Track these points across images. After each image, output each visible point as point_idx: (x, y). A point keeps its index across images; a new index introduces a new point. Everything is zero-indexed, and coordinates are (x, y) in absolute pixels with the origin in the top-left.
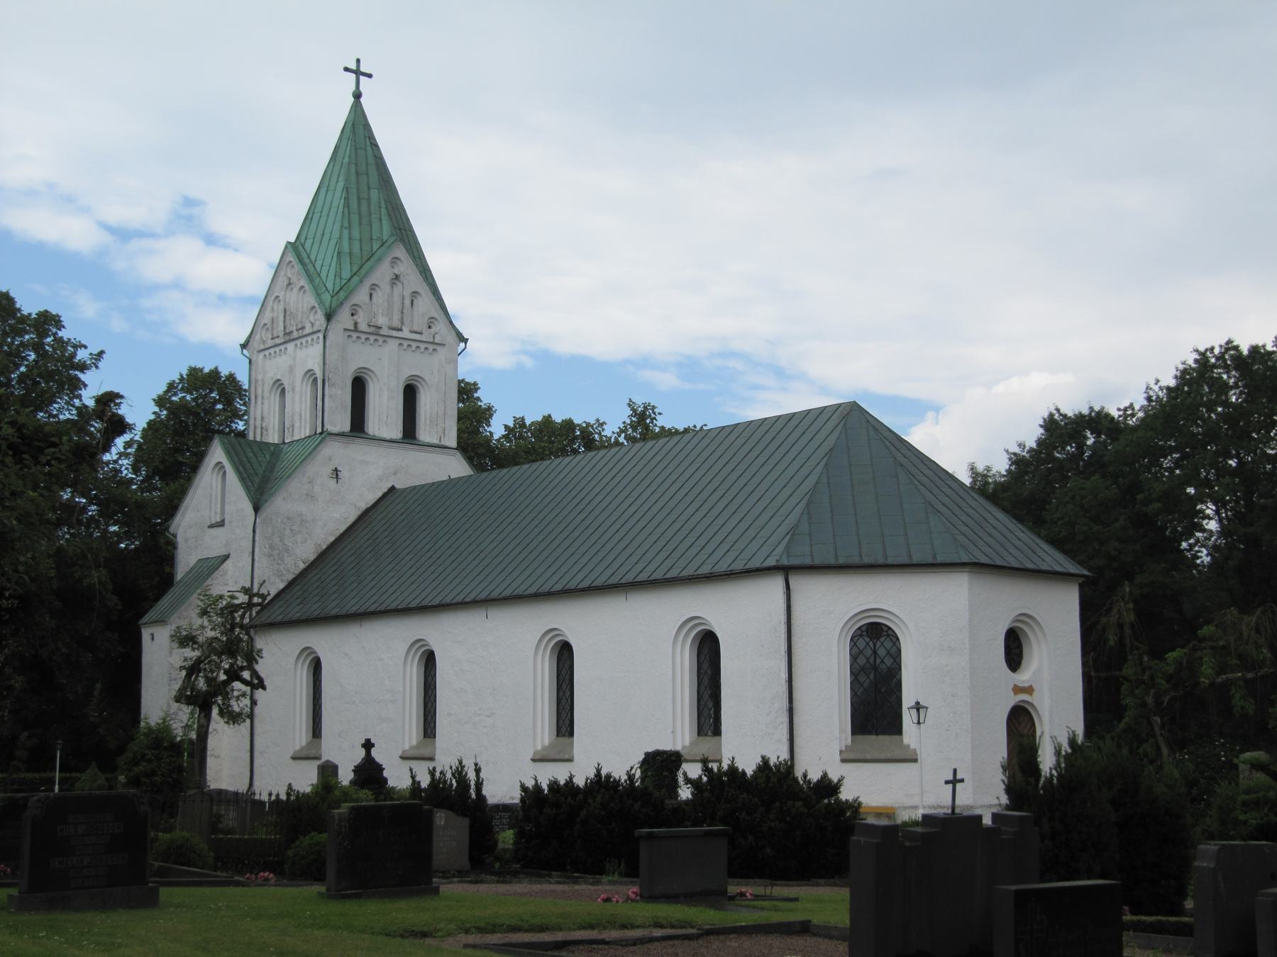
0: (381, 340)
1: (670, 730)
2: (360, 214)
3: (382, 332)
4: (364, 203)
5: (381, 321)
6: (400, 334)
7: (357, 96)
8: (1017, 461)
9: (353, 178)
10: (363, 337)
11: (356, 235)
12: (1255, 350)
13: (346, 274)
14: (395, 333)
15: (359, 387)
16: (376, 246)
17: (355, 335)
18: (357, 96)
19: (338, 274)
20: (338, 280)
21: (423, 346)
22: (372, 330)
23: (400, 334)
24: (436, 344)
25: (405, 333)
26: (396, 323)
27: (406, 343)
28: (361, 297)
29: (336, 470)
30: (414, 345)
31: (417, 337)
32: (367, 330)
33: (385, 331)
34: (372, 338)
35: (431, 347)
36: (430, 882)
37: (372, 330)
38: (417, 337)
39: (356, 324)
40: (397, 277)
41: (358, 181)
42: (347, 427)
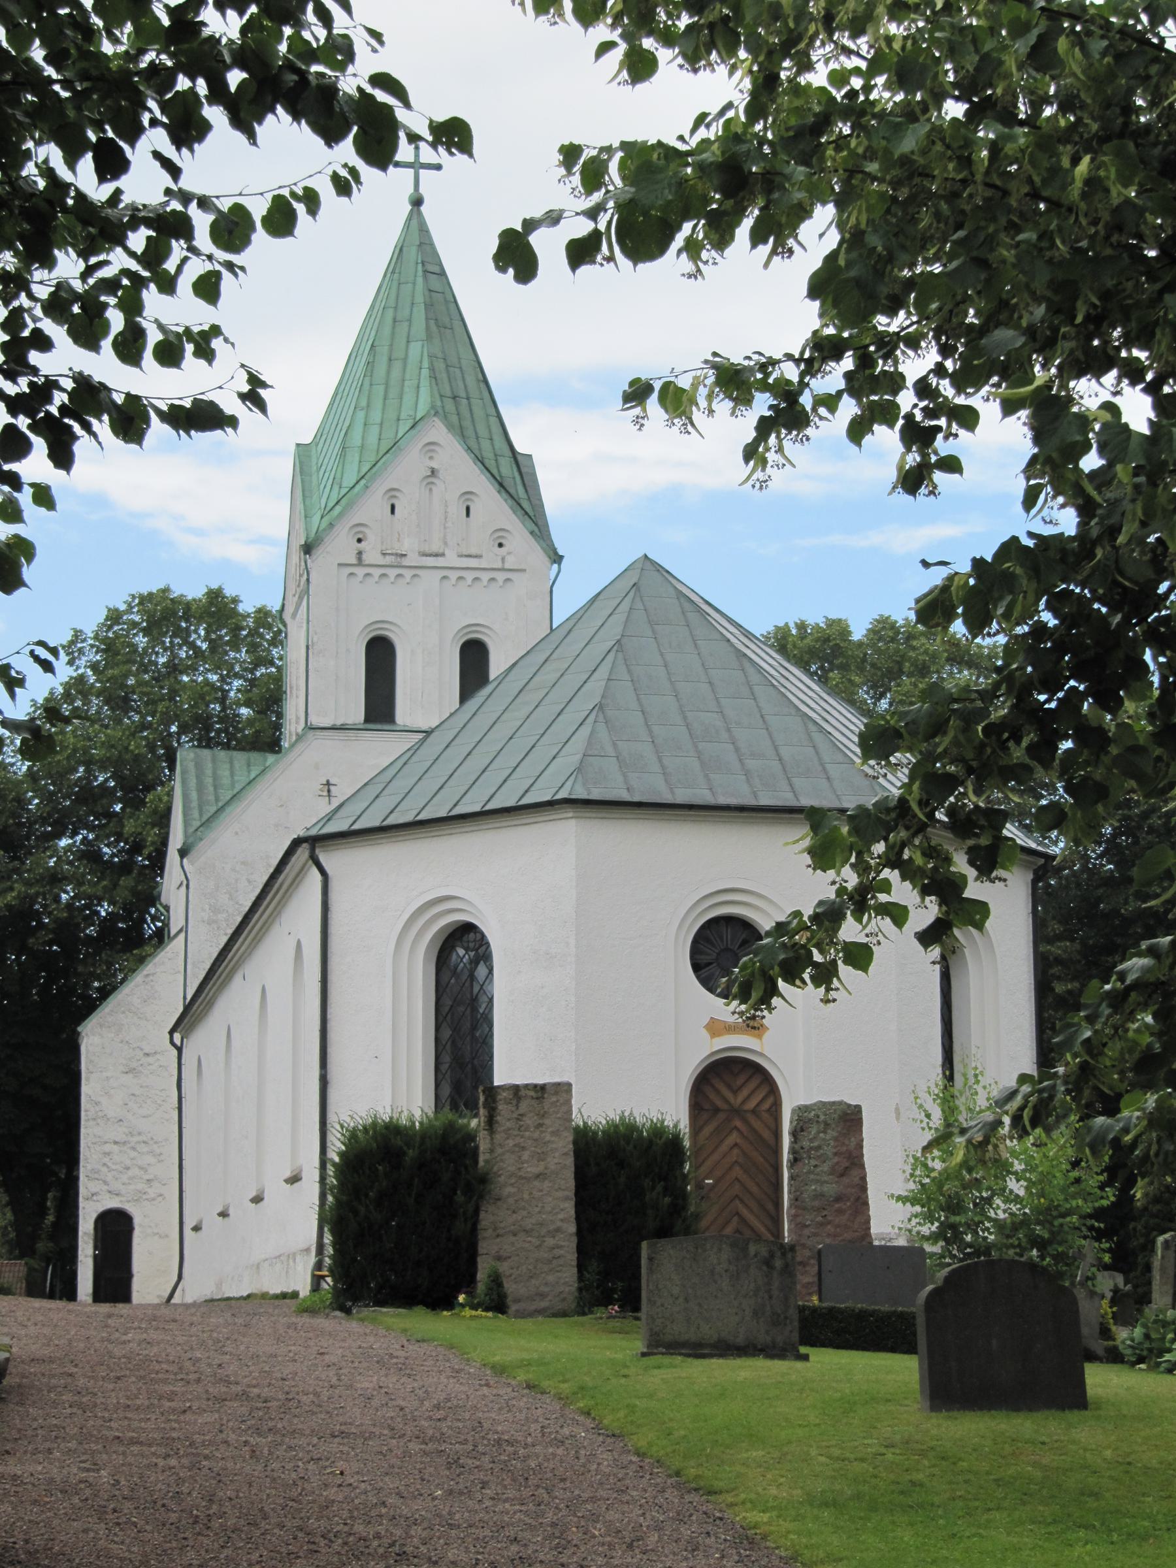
0: (408, 574)
1: (758, 716)
2: (387, 385)
3: (406, 562)
4: (397, 366)
5: (409, 545)
6: (440, 562)
7: (417, 202)
8: (79, 1034)
9: (387, 330)
10: (377, 572)
11: (376, 416)
12: (1126, 425)
13: (350, 479)
14: (430, 562)
15: (380, 655)
16: (404, 427)
17: (360, 572)
18: (417, 202)
19: (337, 482)
20: (336, 487)
21: (485, 577)
22: (389, 560)
23: (440, 562)
24: (508, 573)
25: (451, 559)
26: (435, 547)
27: (453, 575)
28: (371, 509)
29: (328, 783)
30: (470, 576)
31: (473, 563)
32: (381, 561)
33: (413, 559)
34: (392, 573)
35: (501, 576)
36: (914, 443)
37: (389, 560)
38: (473, 563)
39: (360, 553)
40: (433, 472)
41: (393, 334)
42: (357, 713)
